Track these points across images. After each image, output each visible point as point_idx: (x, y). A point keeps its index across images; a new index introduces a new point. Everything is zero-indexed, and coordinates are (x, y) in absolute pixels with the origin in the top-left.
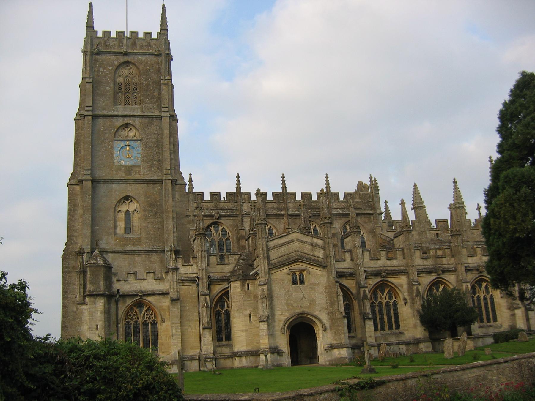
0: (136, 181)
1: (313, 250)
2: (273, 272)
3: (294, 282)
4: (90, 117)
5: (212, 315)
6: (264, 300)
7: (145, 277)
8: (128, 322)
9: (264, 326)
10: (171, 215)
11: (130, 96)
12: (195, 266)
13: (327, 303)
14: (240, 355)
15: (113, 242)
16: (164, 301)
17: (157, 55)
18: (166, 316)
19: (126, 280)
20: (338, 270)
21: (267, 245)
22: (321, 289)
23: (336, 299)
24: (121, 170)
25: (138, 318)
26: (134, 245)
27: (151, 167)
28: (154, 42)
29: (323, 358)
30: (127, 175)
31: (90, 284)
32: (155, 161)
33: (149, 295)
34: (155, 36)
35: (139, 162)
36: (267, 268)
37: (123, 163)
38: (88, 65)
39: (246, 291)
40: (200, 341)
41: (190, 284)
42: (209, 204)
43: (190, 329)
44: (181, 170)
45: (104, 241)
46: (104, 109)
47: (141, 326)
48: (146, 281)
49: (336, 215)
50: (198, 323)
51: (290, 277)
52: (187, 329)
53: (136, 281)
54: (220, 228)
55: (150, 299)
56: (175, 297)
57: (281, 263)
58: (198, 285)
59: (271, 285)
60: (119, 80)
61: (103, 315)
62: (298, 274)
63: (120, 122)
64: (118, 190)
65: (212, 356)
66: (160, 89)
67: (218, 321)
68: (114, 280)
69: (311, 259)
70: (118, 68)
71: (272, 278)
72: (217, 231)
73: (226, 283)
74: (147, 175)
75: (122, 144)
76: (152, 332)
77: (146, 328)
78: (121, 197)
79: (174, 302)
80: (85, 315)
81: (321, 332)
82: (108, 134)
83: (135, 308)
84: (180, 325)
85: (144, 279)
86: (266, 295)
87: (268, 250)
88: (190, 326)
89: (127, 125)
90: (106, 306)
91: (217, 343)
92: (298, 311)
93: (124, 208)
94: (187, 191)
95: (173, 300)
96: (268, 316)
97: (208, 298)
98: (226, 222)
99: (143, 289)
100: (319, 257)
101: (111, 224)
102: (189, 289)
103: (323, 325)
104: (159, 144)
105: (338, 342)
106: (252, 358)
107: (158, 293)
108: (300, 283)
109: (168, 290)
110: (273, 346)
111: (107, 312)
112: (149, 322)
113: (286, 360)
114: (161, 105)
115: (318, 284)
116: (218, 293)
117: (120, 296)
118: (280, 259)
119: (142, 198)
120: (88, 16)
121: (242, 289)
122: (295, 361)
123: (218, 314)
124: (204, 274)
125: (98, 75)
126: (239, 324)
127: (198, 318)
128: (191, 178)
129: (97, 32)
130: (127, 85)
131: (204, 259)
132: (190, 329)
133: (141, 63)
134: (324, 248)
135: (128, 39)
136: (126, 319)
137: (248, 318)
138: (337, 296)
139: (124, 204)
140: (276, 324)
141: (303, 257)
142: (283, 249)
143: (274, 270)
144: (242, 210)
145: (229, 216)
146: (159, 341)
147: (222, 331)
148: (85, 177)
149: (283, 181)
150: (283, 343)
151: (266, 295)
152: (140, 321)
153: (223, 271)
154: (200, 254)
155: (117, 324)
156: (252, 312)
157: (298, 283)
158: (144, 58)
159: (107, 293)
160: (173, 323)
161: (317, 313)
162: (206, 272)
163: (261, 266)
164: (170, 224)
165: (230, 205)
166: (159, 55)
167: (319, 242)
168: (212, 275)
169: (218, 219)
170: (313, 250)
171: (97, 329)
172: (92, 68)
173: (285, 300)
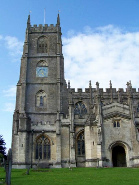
0: (45, 84)
1: (124, 111)
2: (104, 121)
3: (115, 126)
4: (27, 58)
5: (76, 142)
6: (100, 134)
7: (46, 124)
8: (37, 144)
9: (99, 147)
10: (59, 98)
11: (44, 49)
12: (68, 119)
13: (131, 136)
14: (88, 161)
15: (34, 110)
16: (54, 135)
17: (55, 33)
18: (55, 142)
19: (37, 125)
20: (136, 122)
21: (101, 108)
22: (128, 129)
23: (135, 134)
24: (39, 79)
25: (42, 142)
26: (43, 111)
27: (52, 77)
28: (54, 28)
29: (129, 164)
30: (41, 81)
31: (20, 126)
32: (54, 75)
33: (47, 132)
34: (55, 26)
35: (47, 75)
36: (101, 119)
37: (40, 76)
38: (27, 38)
39: (92, 131)
40: (70, 154)
41: (66, 127)
42: (77, 94)
43: (65, 148)
44: (65, 79)
45: (31, 109)
46: (33, 55)
47: (43, 146)
48: (46, 126)
49: (135, 98)
50: (69, 145)
51: (113, 123)
52: (64, 148)
53: (41, 126)
54: (82, 104)
55: (47, 134)
56: (59, 133)
57: (108, 117)
58: (69, 128)
59: (103, 127)
60: (40, 43)
61: (25, 140)
62: (116, 122)
63: (39, 60)
64: (39, 87)
65: (75, 161)
66: (56, 46)
67: (79, 145)
68: (32, 125)
69: (123, 115)
70: (39, 38)
71: (104, 124)
72: (81, 105)
73: (83, 127)
74: (50, 81)
75: (40, 68)
76: (48, 149)
77: (45, 147)
78: (39, 90)
79: (58, 135)
80: (17, 140)
81: (128, 151)
82: (35, 65)
83: (41, 138)
84: (60, 146)
85: (45, 125)
86: (101, 132)
87: (102, 110)
88: (65, 147)
89: (42, 61)
90: (27, 136)
91: (78, 155)
92: (116, 140)
93: (40, 95)
94: (67, 88)
95: (57, 135)
96: (101, 143)
97: (74, 134)
98: (85, 102)
99: (44, 129)
100: (127, 114)
101: (34, 102)
102: (66, 130)
103: (129, 147)
104: (55, 68)
105: (136, 156)
106: (94, 163)
107: (51, 131)
108: (118, 127)
109: (56, 130)
110: (104, 157)
111: (27, 139)
112: (47, 144)
113: (110, 163)
114: (56, 52)
115: (126, 127)
116: (79, 132)
117: (34, 132)
118: (108, 115)
119: (48, 91)
120: (28, 20)
121: (90, 130)
122: (115, 165)
123: (79, 141)
124: (72, 123)
125: (31, 42)
126: (88, 146)
127: (69, 143)
128: (69, 82)
129: (31, 25)
130: (43, 45)
131: (72, 116)
132: (65, 148)
133: (49, 36)
134: (129, 110)
135: (44, 27)
136: (36, 143)
137: (93, 144)
138: (136, 133)
139: (40, 94)
140: (106, 146)
141: (119, 114)
142: (109, 110)
143: (105, 120)
144: (92, 96)
145: (86, 99)
146: (51, 153)
147: (80, 149)
148: (23, 82)
149: (111, 83)
150: (109, 155)
151: (101, 132)
152: (43, 144)
153: (81, 122)
154: (71, 113)
155: (32, 145)
156: (95, 141)
157: (117, 126)
158: (50, 34)
159: (28, 130)
160: (57, 145)
161: (126, 141)
162: (73, 122)
163: (98, 118)
164: (59, 101)
165: (87, 94)
166: (56, 32)
167: (127, 107)
168: (76, 123)
169: (81, 100)
170: (124, 111)
171: (22, 146)
172: (29, 39)
173: (110, 134)
